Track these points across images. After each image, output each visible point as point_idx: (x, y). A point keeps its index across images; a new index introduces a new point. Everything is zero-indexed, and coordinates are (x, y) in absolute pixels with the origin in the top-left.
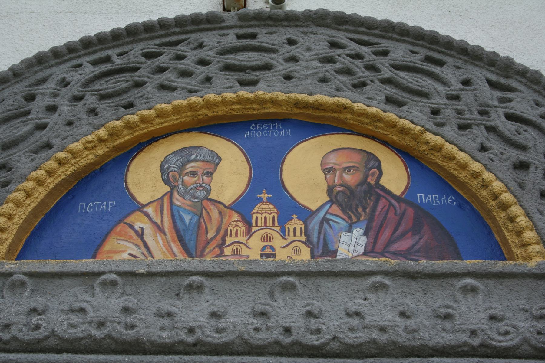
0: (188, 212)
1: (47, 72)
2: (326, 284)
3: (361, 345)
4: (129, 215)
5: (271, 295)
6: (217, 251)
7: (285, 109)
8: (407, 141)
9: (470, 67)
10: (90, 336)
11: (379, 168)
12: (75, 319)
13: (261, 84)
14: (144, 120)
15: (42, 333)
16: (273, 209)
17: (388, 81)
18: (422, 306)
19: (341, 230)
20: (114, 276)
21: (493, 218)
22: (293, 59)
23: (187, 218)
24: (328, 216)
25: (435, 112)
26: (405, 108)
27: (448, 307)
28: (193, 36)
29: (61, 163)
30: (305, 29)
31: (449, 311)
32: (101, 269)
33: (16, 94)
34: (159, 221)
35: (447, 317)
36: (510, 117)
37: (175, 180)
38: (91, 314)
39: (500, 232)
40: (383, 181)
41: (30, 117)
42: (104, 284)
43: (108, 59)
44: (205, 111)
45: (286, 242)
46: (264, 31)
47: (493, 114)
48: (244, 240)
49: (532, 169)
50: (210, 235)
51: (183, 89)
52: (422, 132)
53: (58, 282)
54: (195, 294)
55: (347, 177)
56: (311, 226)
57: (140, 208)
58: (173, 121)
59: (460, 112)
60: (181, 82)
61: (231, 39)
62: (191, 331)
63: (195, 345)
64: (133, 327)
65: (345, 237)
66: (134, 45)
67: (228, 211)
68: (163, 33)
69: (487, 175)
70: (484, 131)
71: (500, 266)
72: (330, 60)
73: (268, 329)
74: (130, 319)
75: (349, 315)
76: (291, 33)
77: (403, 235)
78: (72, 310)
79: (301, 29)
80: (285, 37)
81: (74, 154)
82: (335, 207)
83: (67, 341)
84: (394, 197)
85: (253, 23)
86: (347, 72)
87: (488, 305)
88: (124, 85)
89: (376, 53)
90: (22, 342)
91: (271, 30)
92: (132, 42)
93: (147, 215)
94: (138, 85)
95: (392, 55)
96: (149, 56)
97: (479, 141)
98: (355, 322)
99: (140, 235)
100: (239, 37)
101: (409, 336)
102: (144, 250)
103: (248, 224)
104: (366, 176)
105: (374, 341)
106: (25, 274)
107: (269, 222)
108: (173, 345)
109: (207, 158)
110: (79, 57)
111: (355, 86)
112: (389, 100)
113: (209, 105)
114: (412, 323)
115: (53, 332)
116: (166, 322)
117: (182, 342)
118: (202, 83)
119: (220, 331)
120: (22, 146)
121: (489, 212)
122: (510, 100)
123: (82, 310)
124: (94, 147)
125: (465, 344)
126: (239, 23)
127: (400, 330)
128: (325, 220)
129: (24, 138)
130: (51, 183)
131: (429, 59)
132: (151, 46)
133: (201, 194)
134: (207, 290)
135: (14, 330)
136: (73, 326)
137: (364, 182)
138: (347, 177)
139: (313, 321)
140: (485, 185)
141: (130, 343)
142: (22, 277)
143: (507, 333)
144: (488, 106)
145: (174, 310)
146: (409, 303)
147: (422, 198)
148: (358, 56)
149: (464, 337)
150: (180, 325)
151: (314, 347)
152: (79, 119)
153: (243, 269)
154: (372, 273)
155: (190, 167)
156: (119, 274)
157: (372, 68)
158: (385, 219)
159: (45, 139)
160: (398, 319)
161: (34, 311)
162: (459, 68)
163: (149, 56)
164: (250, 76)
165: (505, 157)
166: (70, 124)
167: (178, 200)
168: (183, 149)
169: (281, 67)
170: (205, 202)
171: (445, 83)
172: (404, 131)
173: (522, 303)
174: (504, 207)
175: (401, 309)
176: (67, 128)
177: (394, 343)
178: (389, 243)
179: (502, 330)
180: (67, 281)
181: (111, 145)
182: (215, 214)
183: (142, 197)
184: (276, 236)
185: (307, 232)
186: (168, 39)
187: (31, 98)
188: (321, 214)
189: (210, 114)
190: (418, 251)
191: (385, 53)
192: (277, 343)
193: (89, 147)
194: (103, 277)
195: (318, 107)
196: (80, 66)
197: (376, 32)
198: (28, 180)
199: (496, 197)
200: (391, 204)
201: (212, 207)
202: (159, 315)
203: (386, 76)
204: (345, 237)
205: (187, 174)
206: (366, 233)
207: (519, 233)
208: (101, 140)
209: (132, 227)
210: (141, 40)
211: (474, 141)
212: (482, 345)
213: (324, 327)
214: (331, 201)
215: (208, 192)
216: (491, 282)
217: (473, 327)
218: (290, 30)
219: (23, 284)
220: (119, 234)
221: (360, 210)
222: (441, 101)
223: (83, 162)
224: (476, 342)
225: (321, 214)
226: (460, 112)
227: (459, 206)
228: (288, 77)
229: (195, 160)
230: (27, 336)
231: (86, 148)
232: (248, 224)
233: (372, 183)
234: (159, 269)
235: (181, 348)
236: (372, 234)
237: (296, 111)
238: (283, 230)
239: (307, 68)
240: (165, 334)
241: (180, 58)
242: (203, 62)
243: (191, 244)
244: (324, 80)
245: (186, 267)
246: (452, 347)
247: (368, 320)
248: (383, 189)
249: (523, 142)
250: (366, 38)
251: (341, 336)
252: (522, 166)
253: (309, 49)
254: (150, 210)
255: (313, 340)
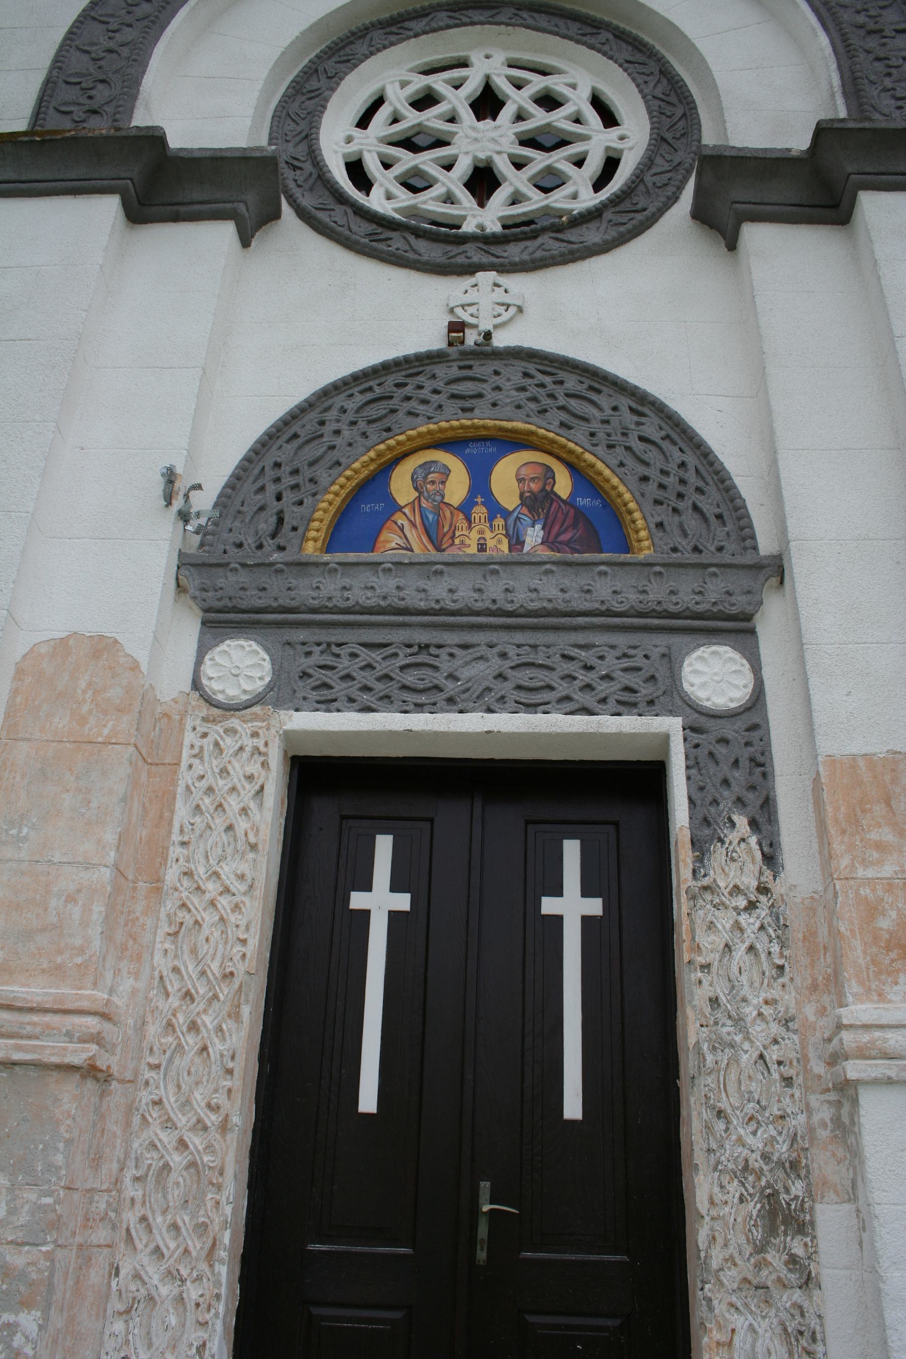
0: (431, 512)
1: (330, 402)
2: (518, 569)
3: (537, 610)
4: (393, 515)
5: (484, 577)
6: (450, 541)
7: (492, 433)
8: (573, 459)
9: (619, 396)
10: (379, 605)
11: (553, 478)
12: (369, 594)
13: (477, 412)
14: (399, 443)
15: (351, 603)
16: (484, 510)
17: (562, 408)
18: (574, 584)
19: (528, 526)
20: (390, 565)
21: (623, 518)
22: (498, 388)
23: (430, 517)
24: (520, 516)
25: (592, 435)
26: (572, 431)
27: (589, 585)
28: (428, 368)
29: (348, 479)
30: (506, 362)
31: (590, 587)
32: (382, 561)
33: (312, 420)
34: (413, 519)
35: (588, 591)
36: (642, 439)
37: (421, 487)
38: (378, 591)
39: (626, 528)
40: (556, 489)
41: (324, 440)
42: (384, 570)
43: (370, 389)
44: (439, 435)
45: (493, 535)
46: (478, 363)
47: (630, 436)
48: (466, 533)
49: (651, 481)
50: (446, 530)
51: (424, 415)
52: (583, 453)
53: (356, 568)
54: (438, 577)
55: (532, 485)
56: (509, 523)
57: (400, 509)
58: (419, 442)
59: (609, 435)
60: (421, 409)
61: (454, 372)
62: (438, 601)
63: (440, 610)
64: (403, 599)
65: (530, 531)
66: (388, 377)
67: (456, 511)
68: (407, 366)
69: (622, 489)
70: (624, 451)
71: (624, 557)
72: (523, 389)
73: (483, 600)
74: (401, 594)
75: (530, 591)
76: (496, 365)
77: (566, 530)
78: (367, 588)
79: (504, 362)
80: (492, 369)
81: (356, 471)
82: (524, 508)
83: (366, 608)
84: (562, 500)
85: (469, 357)
86: (534, 399)
87: (613, 583)
88: (384, 412)
89: (555, 383)
90: (340, 608)
91: (482, 362)
92: (386, 375)
93: (405, 514)
94: (393, 411)
95: (566, 385)
96: (398, 385)
97: (619, 458)
98: (534, 595)
99: (402, 529)
100: (460, 368)
101: (565, 605)
102: (405, 540)
103: (469, 521)
104: (545, 485)
105: (545, 608)
106: (337, 563)
107: (483, 520)
108: (428, 610)
109: (442, 471)
110: (351, 388)
111: (539, 412)
112: (562, 424)
113: (441, 430)
114: (567, 596)
115: (357, 602)
116: (422, 595)
117: (432, 609)
118: (436, 410)
119: (454, 601)
120: (322, 462)
121: (621, 513)
122: (643, 424)
123: (372, 588)
124: (368, 465)
125: (597, 609)
126: (460, 357)
127: (560, 601)
128: (518, 518)
129: (321, 457)
130: (343, 493)
131: (591, 388)
132: (399, 377)
133: (438, 498)
134: (446, 574)
135: (334, 601)
136: (368, 598)
137: (543, 489)
138: (532, 485)
139: (509, 595)
140: (620, 495)
141: (402, 610)
142: (335, 565)
143: (622, 602)
144: (628, 429)
145: (426, 587)
146: (566, 582)
147: (581, 502)
148: (542, 385)
149: (597, 605)
150: (431, 598)
151: (509, 612)
152: (356, 441)
153: (467, 560)
154: (545, 563)
155: (431, 477)
156: (392, 563)
157: (552, 396)
158: (556, 517)
159: (335, 459)
160: (560, 594)
161: (344, 588)
162: (611, 396)
163: (398, 385)
164: (467, 404)
165: (634, 472)
166: (350, 445)
167: (424, 504)
168: (425, 463)
169: (489, 396)
170: (441, 505)
171: (600, 409)
172: (571, 452)
173: (633, 582)
174: (630, 512)
175: (561, 587)
176: (349, 449)
177: (556, 609)
178: (558, 535)
179: (619, 600)
180: (361, 568)
181: (379, 462)
182: (448, 514)
183: (402, 501)
184: (487, 530)
185: (506, 527)
186: (411, 371)
187: (322, 423)
188: (515, 514)
189: (443, 436)
190: (575, 541)
191: (561, 383)
192: (488, 609)
193: (365, 465)
194: (383, 566)
195: (514, 431)
196: (352, 395)
197: (556, 365)
198: (329, 493)
199: (625, 505)
200: (560, 506)
201: (446, 509)
202: (418, 590)
203: (561, 404)
204: (530, 531)
205: (429, 483)
206: (543, 528)
207: (637, 532)
208: (372, 460)
209: (396, 524)
210: (392, 373)
211: (616, 458)
212: (607, 610)
213: (515, 599)
214: (522, 504)
215: (443, 497)
216: (616, 568)
217: (602, 599)
218: (496, 363)
219: (336, 570)
220: (388, 529)
221: (540, 510)
222: (596, 426)
223: (362, 476)
224: (604, 608)
225: (515, 514)
226: (609, 435)
227: (604, 507)
228: (494, 405)
229: (433, 472)
230: (343, 605)
231: (363, 467)
232: (469, 521)
233: (549, 489)
234: (417, 560)
235: (432, 612)
236: (547, 529)
237: (500, 433)
238: (491, 526)
239: (507, 397)
240: (422, 604)
241: (420, 387)
242: (436, 392)
243: (434, 536)
244: (519, 407)
245: (433, 559)
246: (590, 611)
247: (542, 594)
248: (555, 494)
249: (647, 460)
250: (548, 369)
251: (525, 605)
252: (645, 479)
253: (509, 380)
254: (406, 510)
255: (509, 607)
